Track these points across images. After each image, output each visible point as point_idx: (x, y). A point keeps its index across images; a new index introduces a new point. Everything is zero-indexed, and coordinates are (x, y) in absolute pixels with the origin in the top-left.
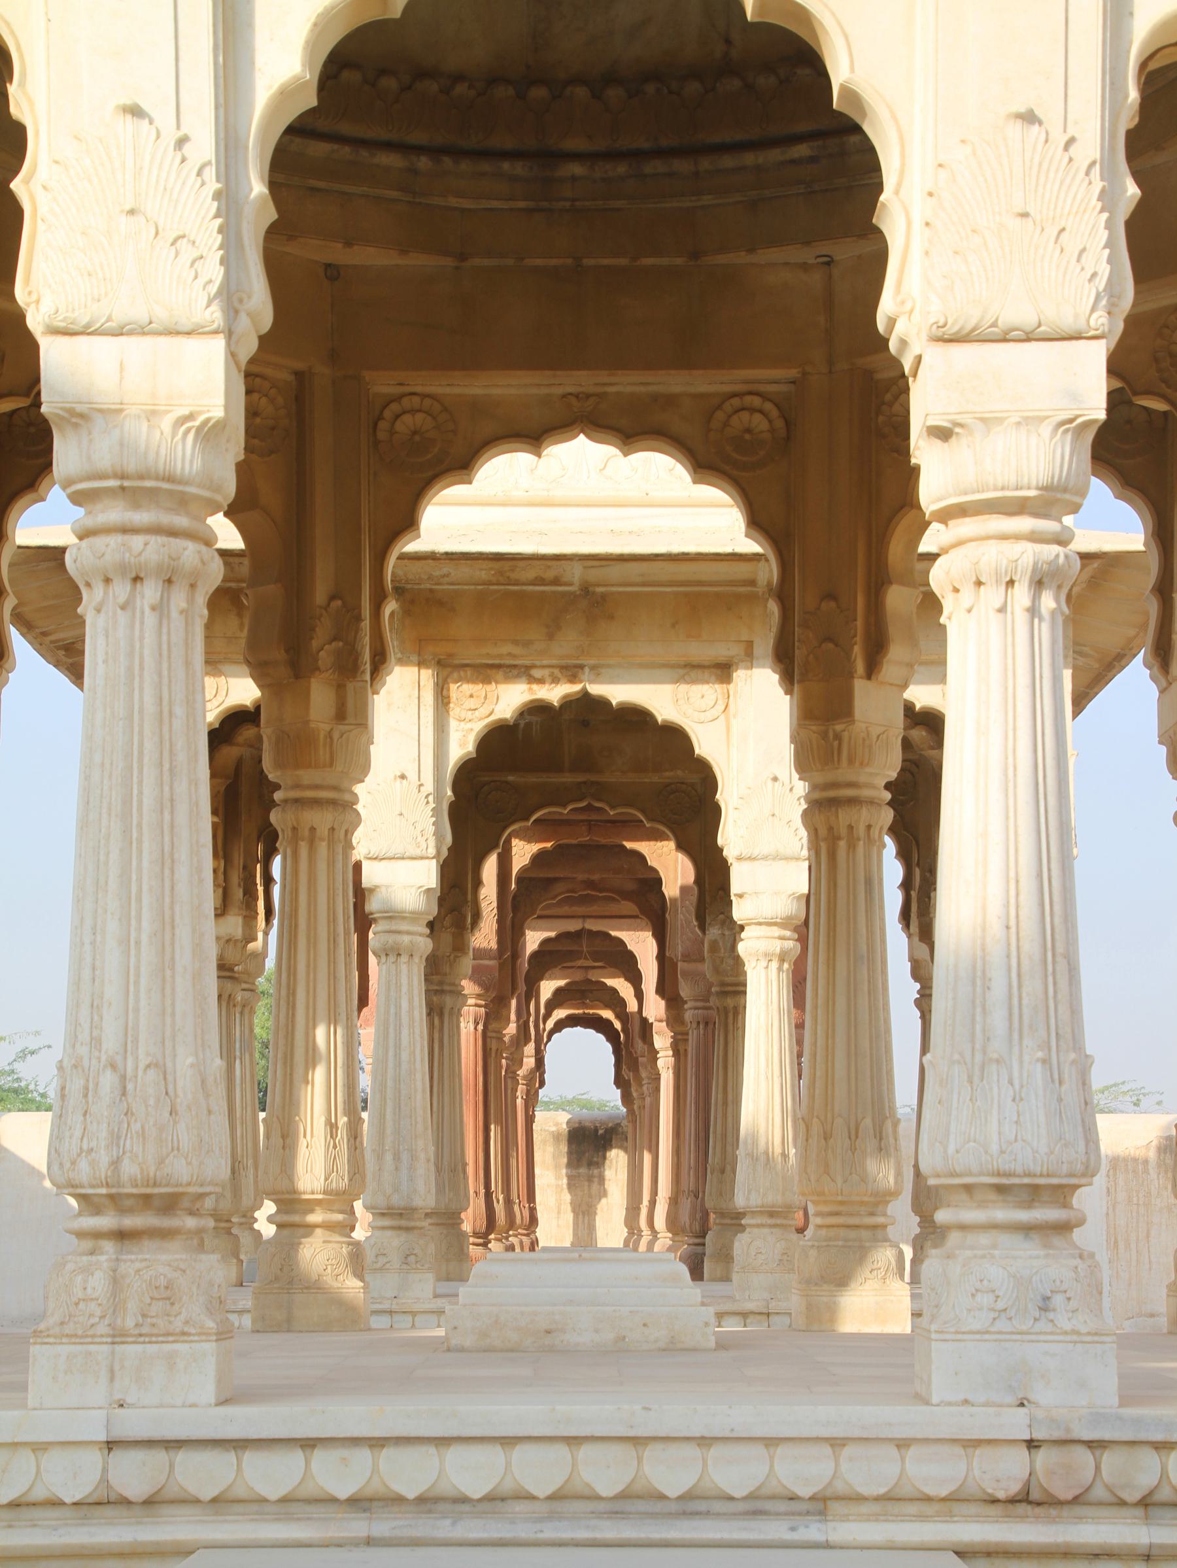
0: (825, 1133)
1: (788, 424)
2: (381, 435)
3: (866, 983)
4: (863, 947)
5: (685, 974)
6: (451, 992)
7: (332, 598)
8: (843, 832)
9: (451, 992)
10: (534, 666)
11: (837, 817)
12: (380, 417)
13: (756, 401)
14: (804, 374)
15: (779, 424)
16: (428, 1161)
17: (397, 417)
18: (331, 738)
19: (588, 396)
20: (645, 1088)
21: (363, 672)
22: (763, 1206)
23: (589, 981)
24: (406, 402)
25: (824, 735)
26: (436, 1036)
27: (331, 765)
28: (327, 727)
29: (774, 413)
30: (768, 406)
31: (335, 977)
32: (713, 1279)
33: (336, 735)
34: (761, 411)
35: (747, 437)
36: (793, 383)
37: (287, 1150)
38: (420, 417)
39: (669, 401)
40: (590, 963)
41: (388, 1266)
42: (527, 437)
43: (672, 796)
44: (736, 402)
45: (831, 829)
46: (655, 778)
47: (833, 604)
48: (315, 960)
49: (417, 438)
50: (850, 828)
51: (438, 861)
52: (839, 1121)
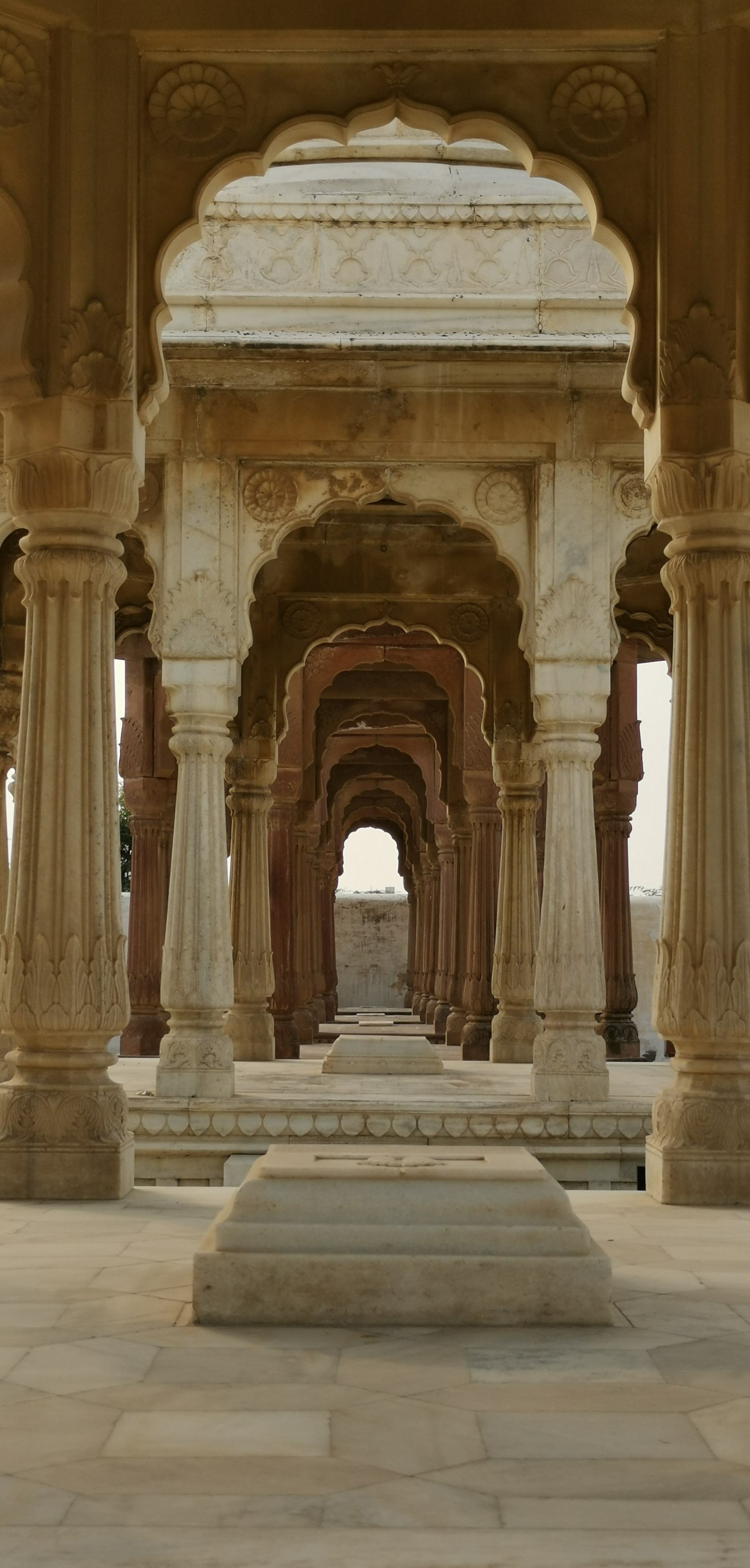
1: (647, 101)
2: (155, 111)
5: (468, 779)
6: (258, 795)
7: (93, 298)
8: (716, 589)
9: (258, 795)
10: (335, 468)
11: (709, 571)
12: (153, 89)
13: (609, 73)
14: (669, 35)
15: (637, 99)
16: (227, 960)
17: (174, 89)
18: (87, 471)
19: (404, 66)
20: (425, 877)
21: (128, 390)
22: (563, 1008)
24: (184, 72)
25: (695, 470)
27: (87, 505)
28: (82, 456)
29: (631, 87)
30: (623, 78)
31: (90, 763)
32: (498, 1061)
33: (93, 467)
34: (613, 84)
35: (597, 115)
36: (654, 51)
37: (28, 975)
38: (201, 89)
39: (503, 72)
40: (379, 775)
41: (185, 1065)
42: (331, 113)
43: (463, 616)
44: (584, 73)
45: (700, 587)
46: (449, 600)
47: (705, 310)
49: (198, 114)
50: (725, 585)
51: (238, 661)
52: (711, 944)
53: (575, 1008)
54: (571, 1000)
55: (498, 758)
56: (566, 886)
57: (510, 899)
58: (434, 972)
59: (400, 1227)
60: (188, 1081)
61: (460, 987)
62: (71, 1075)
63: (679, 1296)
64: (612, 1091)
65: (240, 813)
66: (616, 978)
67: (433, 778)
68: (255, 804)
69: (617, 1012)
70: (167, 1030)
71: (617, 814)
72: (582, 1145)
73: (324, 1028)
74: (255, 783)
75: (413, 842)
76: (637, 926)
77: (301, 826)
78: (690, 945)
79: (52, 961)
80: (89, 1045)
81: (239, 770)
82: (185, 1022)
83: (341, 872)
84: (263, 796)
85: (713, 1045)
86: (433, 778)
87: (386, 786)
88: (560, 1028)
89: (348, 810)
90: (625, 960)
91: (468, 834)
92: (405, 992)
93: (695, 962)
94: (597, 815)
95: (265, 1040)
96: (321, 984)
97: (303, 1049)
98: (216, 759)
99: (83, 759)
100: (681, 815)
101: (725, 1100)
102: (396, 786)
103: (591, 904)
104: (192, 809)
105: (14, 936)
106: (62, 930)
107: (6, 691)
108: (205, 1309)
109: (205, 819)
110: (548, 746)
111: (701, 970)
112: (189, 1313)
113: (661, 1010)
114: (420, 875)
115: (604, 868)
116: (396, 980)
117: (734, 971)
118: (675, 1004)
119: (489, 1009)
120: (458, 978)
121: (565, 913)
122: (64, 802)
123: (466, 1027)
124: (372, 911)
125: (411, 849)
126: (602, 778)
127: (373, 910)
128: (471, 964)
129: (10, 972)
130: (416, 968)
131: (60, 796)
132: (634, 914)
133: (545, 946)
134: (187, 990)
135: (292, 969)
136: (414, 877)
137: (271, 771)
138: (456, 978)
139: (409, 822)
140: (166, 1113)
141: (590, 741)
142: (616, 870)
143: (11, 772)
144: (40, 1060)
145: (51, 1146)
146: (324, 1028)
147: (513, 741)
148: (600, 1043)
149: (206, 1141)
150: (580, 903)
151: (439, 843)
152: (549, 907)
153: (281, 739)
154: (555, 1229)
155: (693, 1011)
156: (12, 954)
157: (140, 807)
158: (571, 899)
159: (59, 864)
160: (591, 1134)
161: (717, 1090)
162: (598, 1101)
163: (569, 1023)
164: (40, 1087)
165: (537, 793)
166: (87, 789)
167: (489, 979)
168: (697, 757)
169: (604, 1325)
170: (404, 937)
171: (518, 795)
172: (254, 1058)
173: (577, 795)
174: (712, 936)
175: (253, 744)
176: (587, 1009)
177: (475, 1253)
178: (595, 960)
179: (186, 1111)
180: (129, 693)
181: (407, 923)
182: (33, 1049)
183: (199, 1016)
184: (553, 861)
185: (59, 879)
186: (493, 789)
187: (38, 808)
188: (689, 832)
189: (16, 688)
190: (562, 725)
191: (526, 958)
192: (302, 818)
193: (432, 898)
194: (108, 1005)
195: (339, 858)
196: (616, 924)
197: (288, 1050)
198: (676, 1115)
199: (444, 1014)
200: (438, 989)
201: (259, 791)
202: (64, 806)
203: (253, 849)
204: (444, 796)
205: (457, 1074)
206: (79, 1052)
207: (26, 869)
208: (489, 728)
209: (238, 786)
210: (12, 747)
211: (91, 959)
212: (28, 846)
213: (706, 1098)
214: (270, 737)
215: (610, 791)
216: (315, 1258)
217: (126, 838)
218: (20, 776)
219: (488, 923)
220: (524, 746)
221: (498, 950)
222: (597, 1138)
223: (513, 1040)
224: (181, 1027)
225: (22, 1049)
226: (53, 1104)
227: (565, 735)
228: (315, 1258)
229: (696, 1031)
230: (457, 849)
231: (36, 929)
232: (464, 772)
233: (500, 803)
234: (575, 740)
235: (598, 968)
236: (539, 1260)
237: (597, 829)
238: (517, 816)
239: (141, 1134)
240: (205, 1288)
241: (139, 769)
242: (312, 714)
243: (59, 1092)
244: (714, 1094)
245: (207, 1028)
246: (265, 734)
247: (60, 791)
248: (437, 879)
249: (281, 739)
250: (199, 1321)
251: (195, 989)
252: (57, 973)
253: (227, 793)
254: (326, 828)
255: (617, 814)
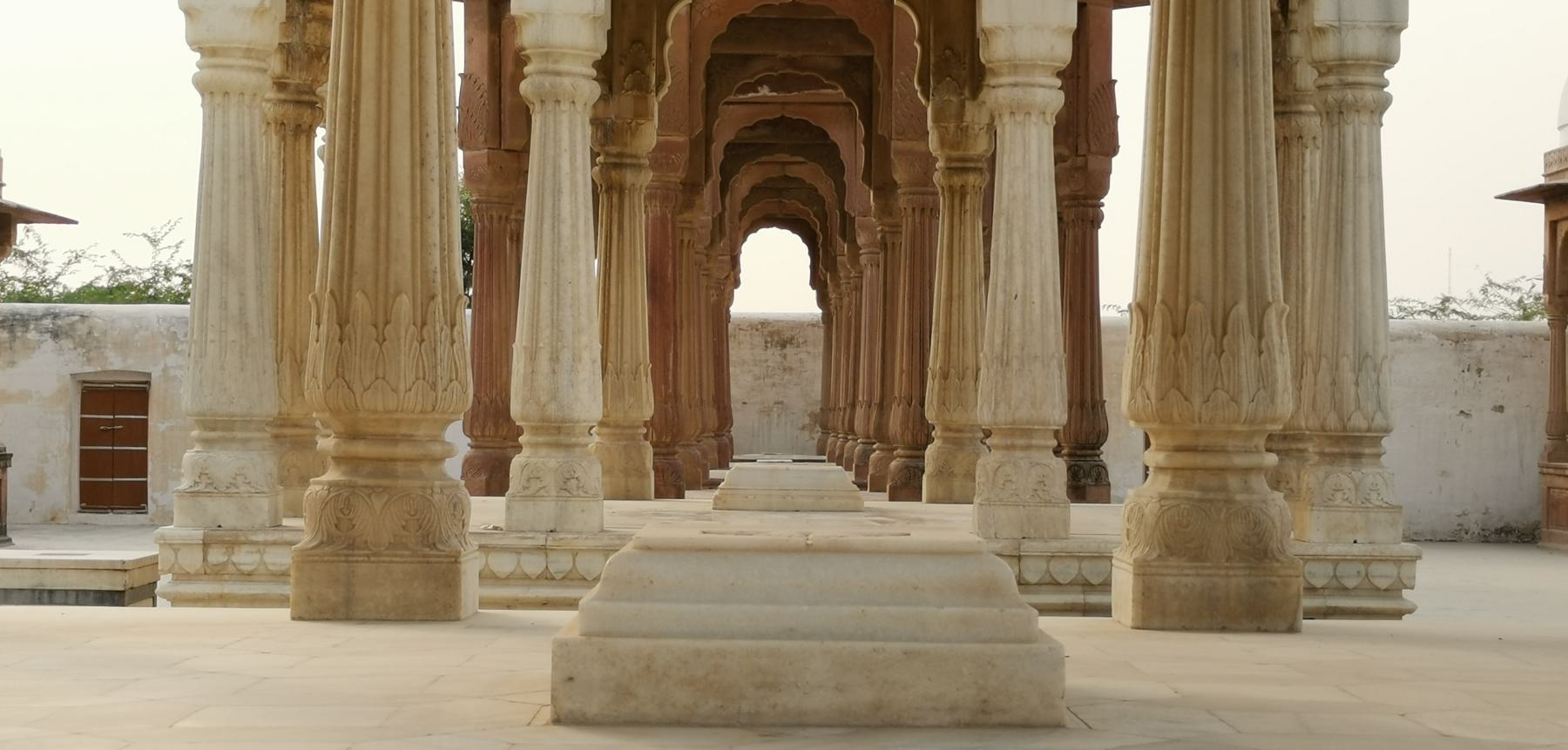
0: (1174, 326)
3: (1241, 95)
4: (1238, 43)
6: (633, 166)
9: (633, 166)
16: (594, 362)
22: (1014, 422)
23: (786, 178)
26: (615, 216)
31: (421, 78)
32: (932, 501)
37: (346, 343)
40: (785, 157)
41: (542, 492)
48: (390, 50)
52: (1196, 307)
53: (1028, 422)
54: (1024, 413)
55: (936, 120)
56: (1018, 269)
57: (950, 298)
58: (853, 406)
59: (805, 608)
60: (546, 511)
61: (887, 425)
62: (400, 467)
63: (1148, 702)
64: (1073, 529)
65: (609, 189)
66: (1082, 405)
67: (854, 156)
68: (629, 177)
69: (1084, 448)
70: (519, 448)
71: (1085, 198)
72: (1038, 593)
73: (714, 474)
74: (628, 150)
75: (828, 241)
76: (1108, 354)
77: (686, 216)
78: (1170, 307)
79: (376, 326)
80: (422, 432)
81: (609, 134)
82: (541, 439)
83: (737, 283)
84: (638, 167)
85: (1197, 434)
86: (854, 156)
87: (793, 171)
88: (1010, 448)
89: (747, 203)
90: (1093, 383)
91: (898, 226)
92: (817, 435)
93: (1177, 330)
94: (1060, 199)
95: (643, 475)
96: (713, 422)
97: (687, 493)
98: (579, 107)
99: (412, 73)
100: (1162, 147)
101: (1211, 501)
102: (807, 171)
103: (1050, 293)
104: (549, 172)
105: (327, 295)
106: (387, 284)
107: (314, 24)
108: (567, 705)
109: (566, 185)
110: (998, 94)
111: (1184, 339)
112: (547, 714)
113: (1133, 390)
114: (838, 286)
115: (1068, 258)
116: (807, 420)
117: (1225, 341)
118: (1150, 383)
119: (920, 437)
120: (882, 408)
121: (1017, 303)
122: (389, 126)
123: (893, 464)
124: (778, 335)
125: (826, 252)
126: (1066, 152)
127: (778, 333)
128: (900, 385)
129: (323, 339)
130: (831, 405)
131: (384, 118)
132: (1105, 339)
133: (992, 344)
134: (544, 399)
135: (675, 390)
136: (830, 289)
137: (649, 137)
138: (881, 407)
139: (824, 218)
140: (517, 551)
141: (1051, 87)
142: (1084, 271)
143: (321, 132)
144: (361, 449)
145: (375, 555)
146: (714, 474)
147: (954, 99)
148: (1059, 466)
149: (568, 587)
150: (1036, 291)
151: (861, 240)
152: (997, 295)
153: (662, 95)
154: (996, 610)
155: (1173, 391)
156: (325, 316)
157: (484, 187)
158: (1025, 286)
159: (383, 204)
160: (1048, 579)
161: (1203, 489)
162: (1056, 538)
163: (1021, 442)
164: (361, 481)
165: (985, 166)
166: (417, 110)
167: (923, 405)
168: (1182, 73)
169: (1056, 726)
170: (817, 367)
171: (959, 167)
172: (628, 497)
173: (1034, 156)
174: (1198, 298)
175: (625, 101)
176: (1043, 424)
177: (899, 639)
178: (1055, 363)
179: (543, 549)
180: (469, 42)
181: (821, 349)
182: (353, 435)
183: (558, 432)
184: (1002, 240)
185: (383, 223)
186: (929, 160)
187: (356, 135)
188: (1171, 168)
189: (325, 20)
190: (1015, 67)
191: (969, 372)
192: (688, 205)
193: (852, 313)
194: (445, 381)
195: (735, 263)
196: (1083, 338)
197: (671, 485)
198: (1151, 520)
199: (865, 455)
200: (859, 424)
201: (634, 161)
202: (389, 132)
203: (627, 233)
204: (867, 178)
205: (882, 512)
206: (409, 439)
207: (342, 211)
208: (924, 82)
209: (607, 154)
210: (323, 100)
211: (424, 324)
212: (344, 182)
213: (1188, 499)
214: (648, 91)
215: (1077, 169)
216: (700, 644)
217: (467, 246)
218: (331, 139)
219: (922, 332)
220: (968, 104)
221: (934, 361)
222: (1055, 584)
223: (952, 475)
224: (536, 445)
225: (339, 435)
226: (378, 504)
227: (1019, 79)
228: (700, 644)
229: (1176, 415)
230: (884, 245)
231: (355, 287)
232: (893, 143)
233: (937, 177)
234: (1032, 85)
235: (1057, 373)
236: (976, 647)
237: (1060, 219)
238: (958, 194)
239: (487, 577)
240: (566, 680)
241: (482, 138)
242: (702, 67)
243: (385, 488)
244: (1197, 494)
245: (569, 447)
246: (641, 87)
247: (384, 112)
248: (858, 288)
249: (662, 95)
250: (557, 721)
251: (554, 398)
252: (381, 340)
253: (593, 164)
254: (719, 221)
255: (1085, 198)
